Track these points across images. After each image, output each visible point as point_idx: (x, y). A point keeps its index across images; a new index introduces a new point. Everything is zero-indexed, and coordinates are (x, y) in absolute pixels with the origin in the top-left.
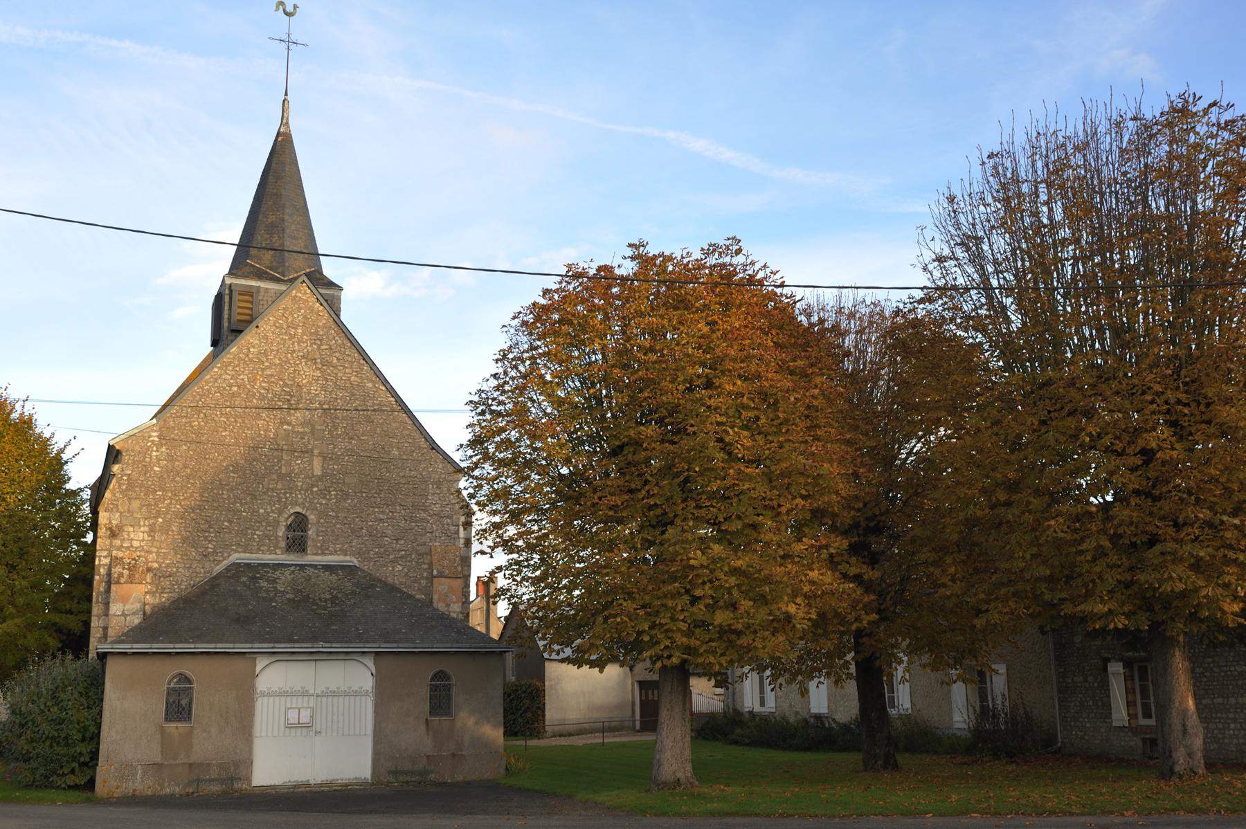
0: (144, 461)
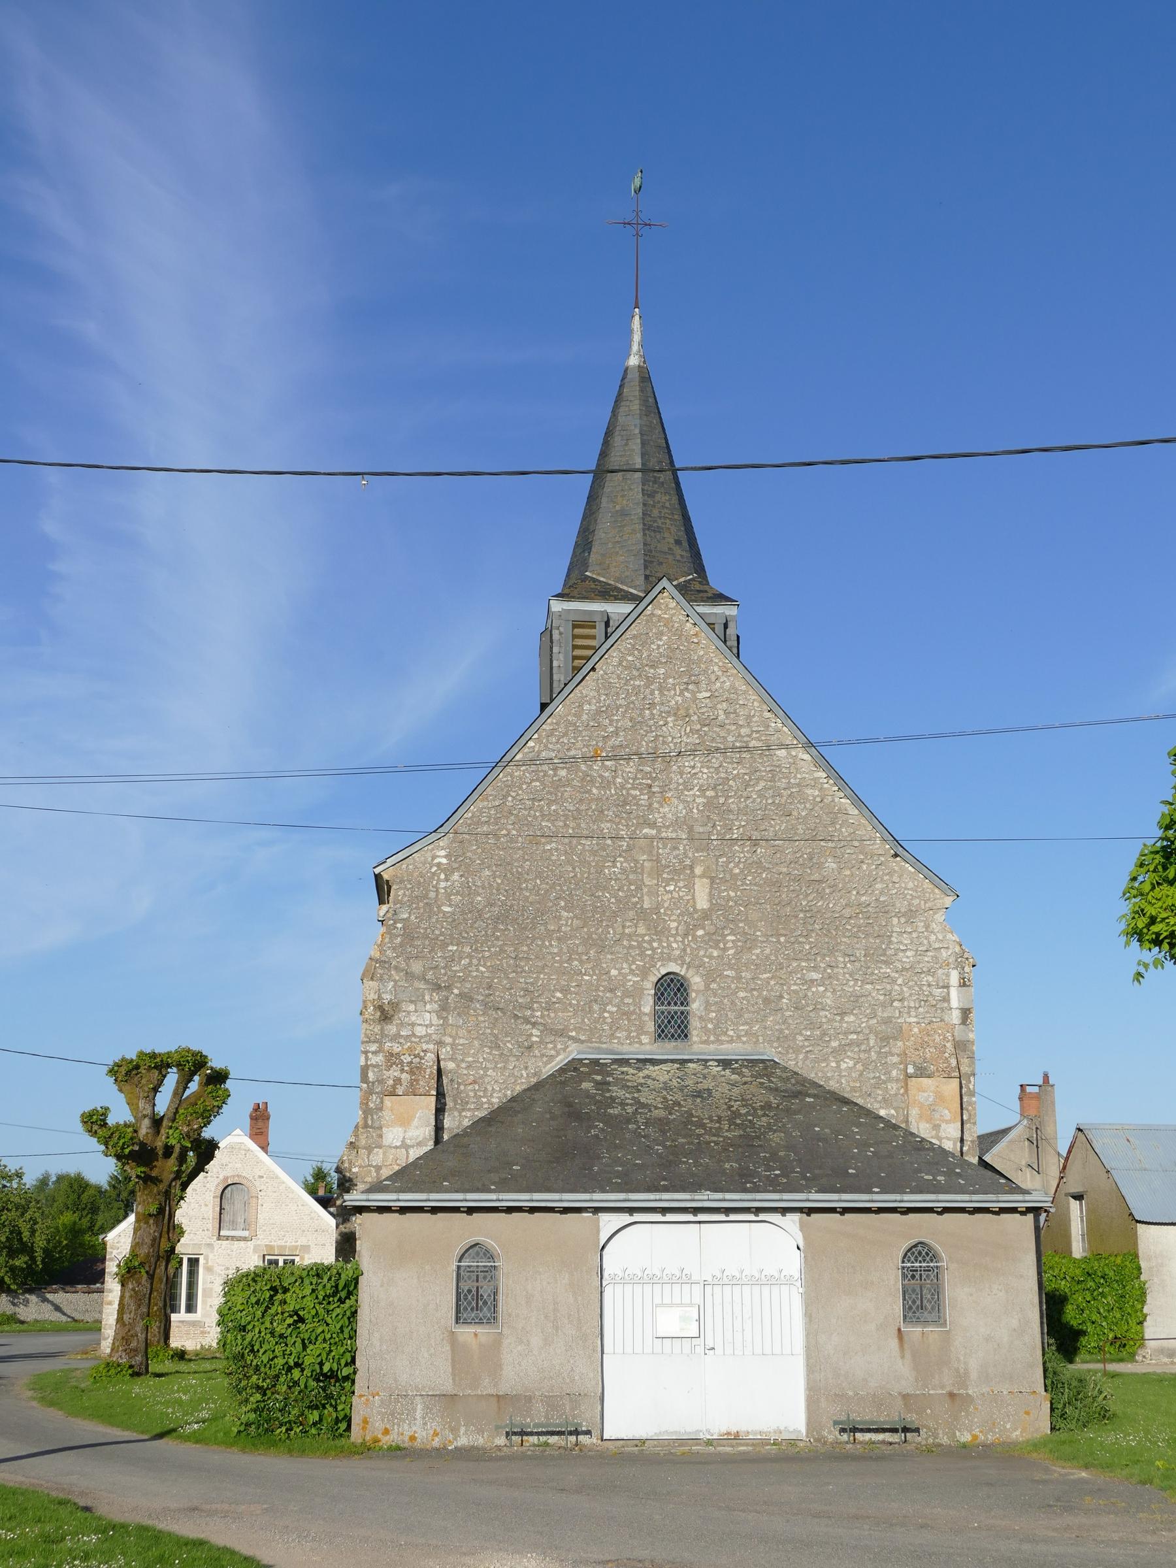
0: (426, 896)
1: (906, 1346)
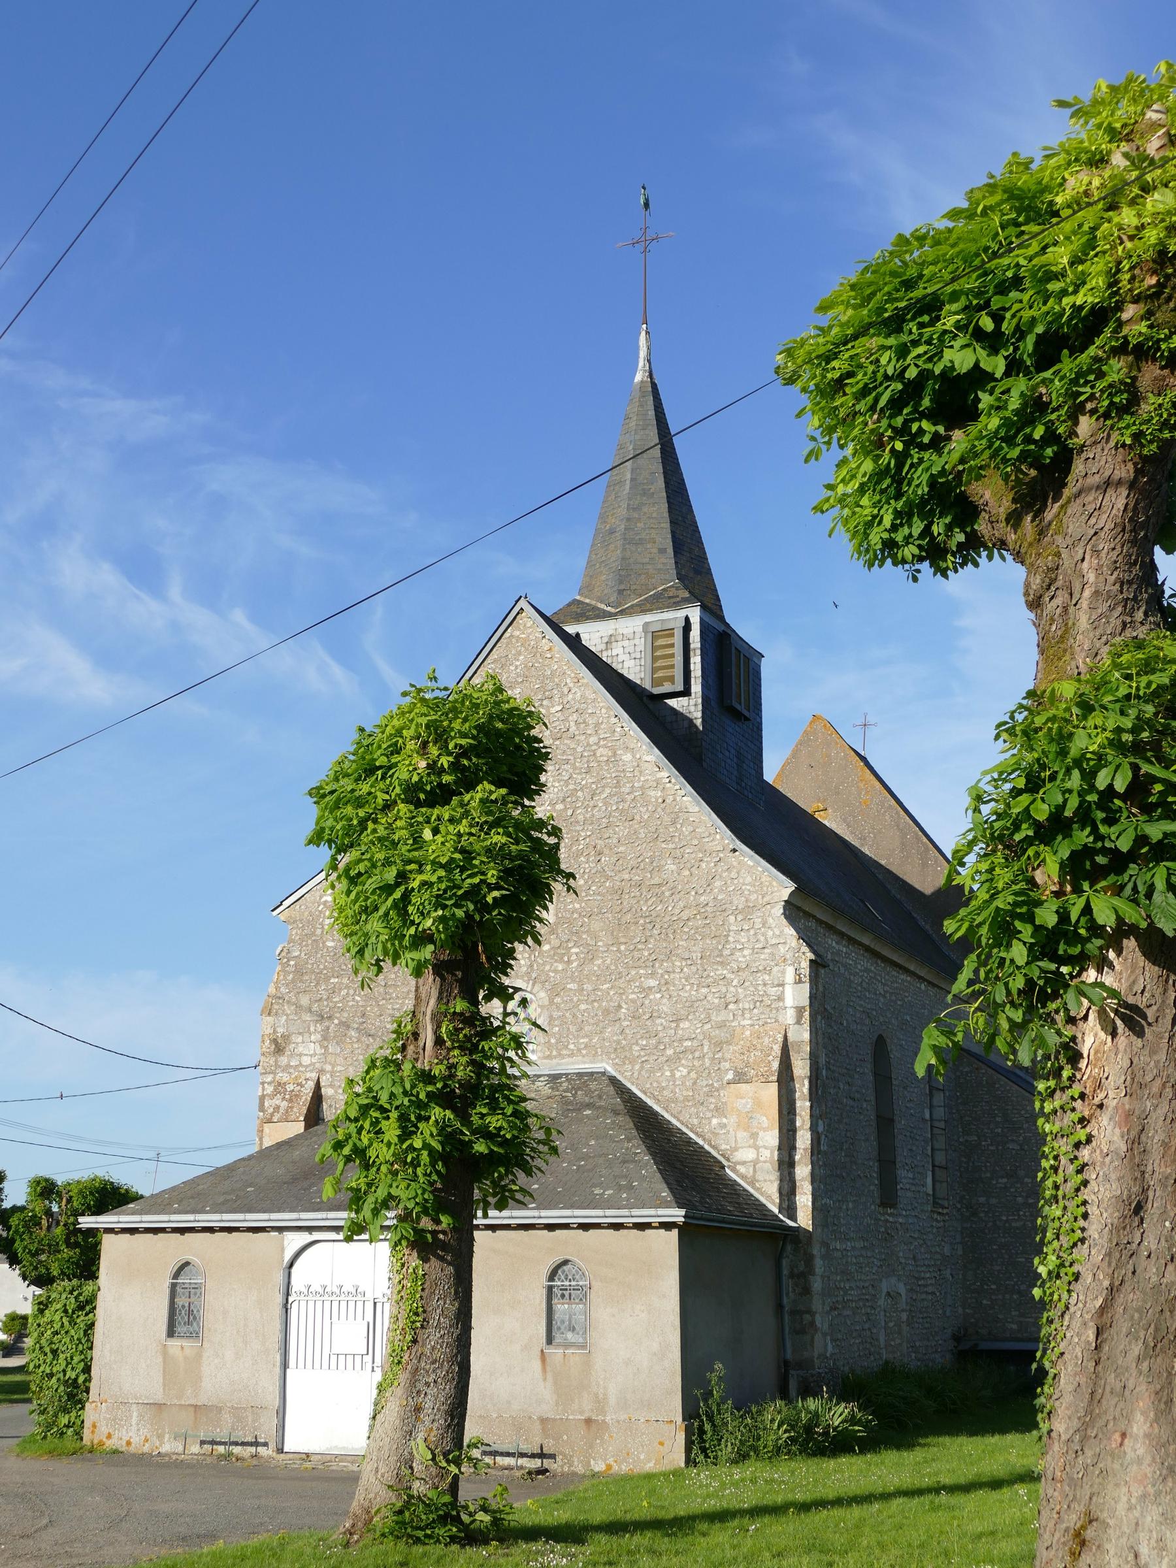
0: (313, 934)
1: (548, 1369)
